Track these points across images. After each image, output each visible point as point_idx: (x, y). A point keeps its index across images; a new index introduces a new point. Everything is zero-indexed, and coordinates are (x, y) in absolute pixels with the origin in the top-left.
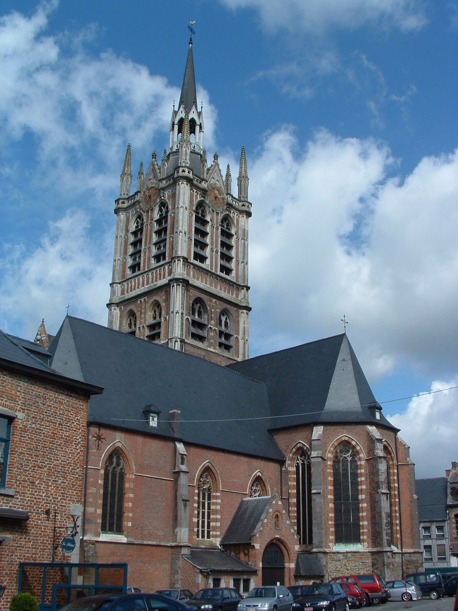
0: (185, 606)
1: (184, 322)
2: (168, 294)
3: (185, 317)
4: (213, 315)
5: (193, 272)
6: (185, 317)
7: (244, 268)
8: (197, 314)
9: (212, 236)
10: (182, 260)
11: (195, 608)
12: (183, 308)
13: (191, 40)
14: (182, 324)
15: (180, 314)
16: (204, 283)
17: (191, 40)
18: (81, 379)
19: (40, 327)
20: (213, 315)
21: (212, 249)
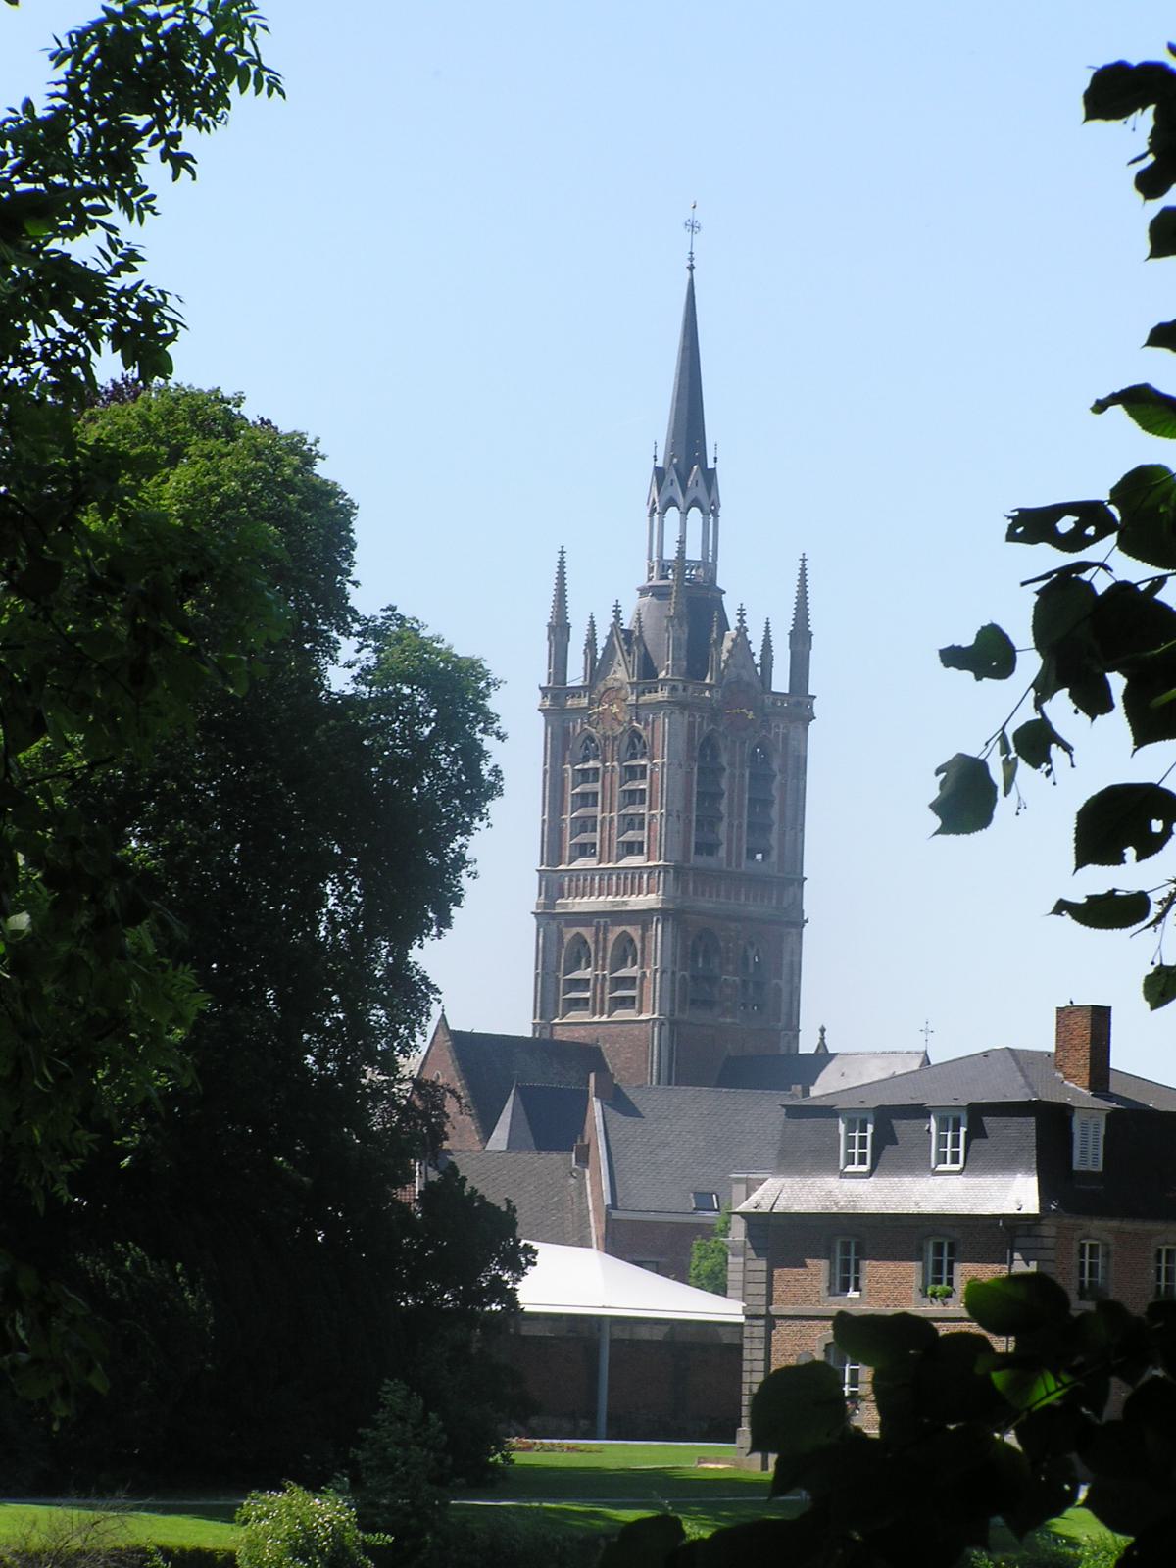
0: (1127, 697)
1: (677, 988)
2: (645, 929)
3: (678, 976)
4: (731, 955)
5: (694, 882)
6: (678, 976)
7: (796, 840)
8: (700, 960)
9: (731, 799)
10: (672, 871)
11: (41, 186)
12: (674, 963)
13: (716, 461)
14: (674, 991)
15: (670, 974)
16: (715, 899)
17: (716, 461)
18: (710, 1533)
19: (440, 1021)
20: (731, 955)
21: (731, 826)
